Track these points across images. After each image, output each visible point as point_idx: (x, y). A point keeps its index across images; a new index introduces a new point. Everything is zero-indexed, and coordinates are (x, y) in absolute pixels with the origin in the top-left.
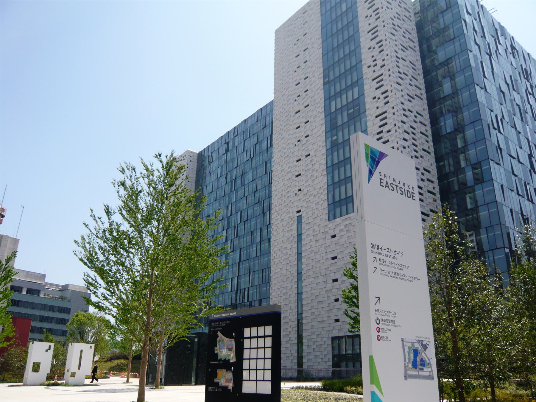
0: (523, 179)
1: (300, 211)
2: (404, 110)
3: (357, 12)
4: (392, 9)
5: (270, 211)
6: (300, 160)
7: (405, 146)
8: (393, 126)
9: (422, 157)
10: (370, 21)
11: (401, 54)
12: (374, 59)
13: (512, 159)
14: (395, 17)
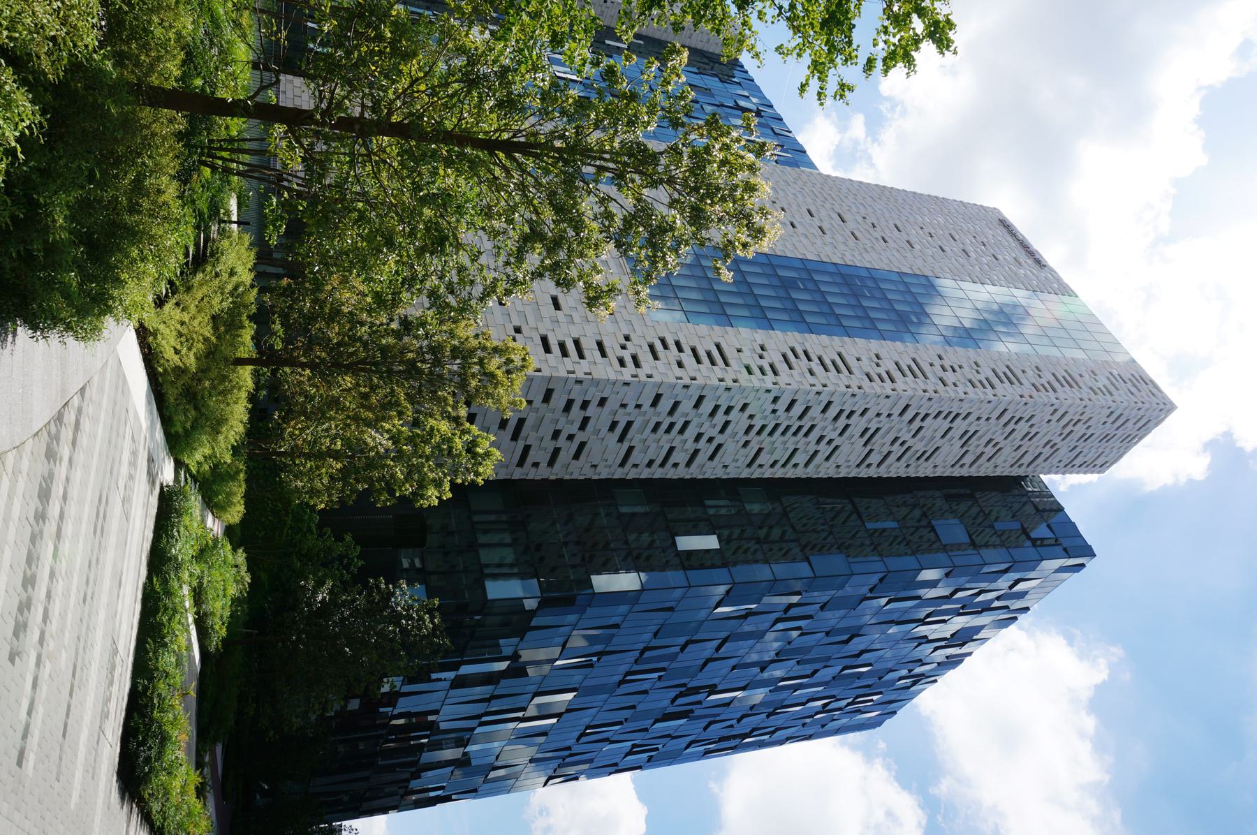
0: (674, 665)
2: (585, 405)
7: (780, 402)
8: (693, 375)
9: (746, 444)
12: (957, 368)
13: (716, 643)
14: (1032, 426)
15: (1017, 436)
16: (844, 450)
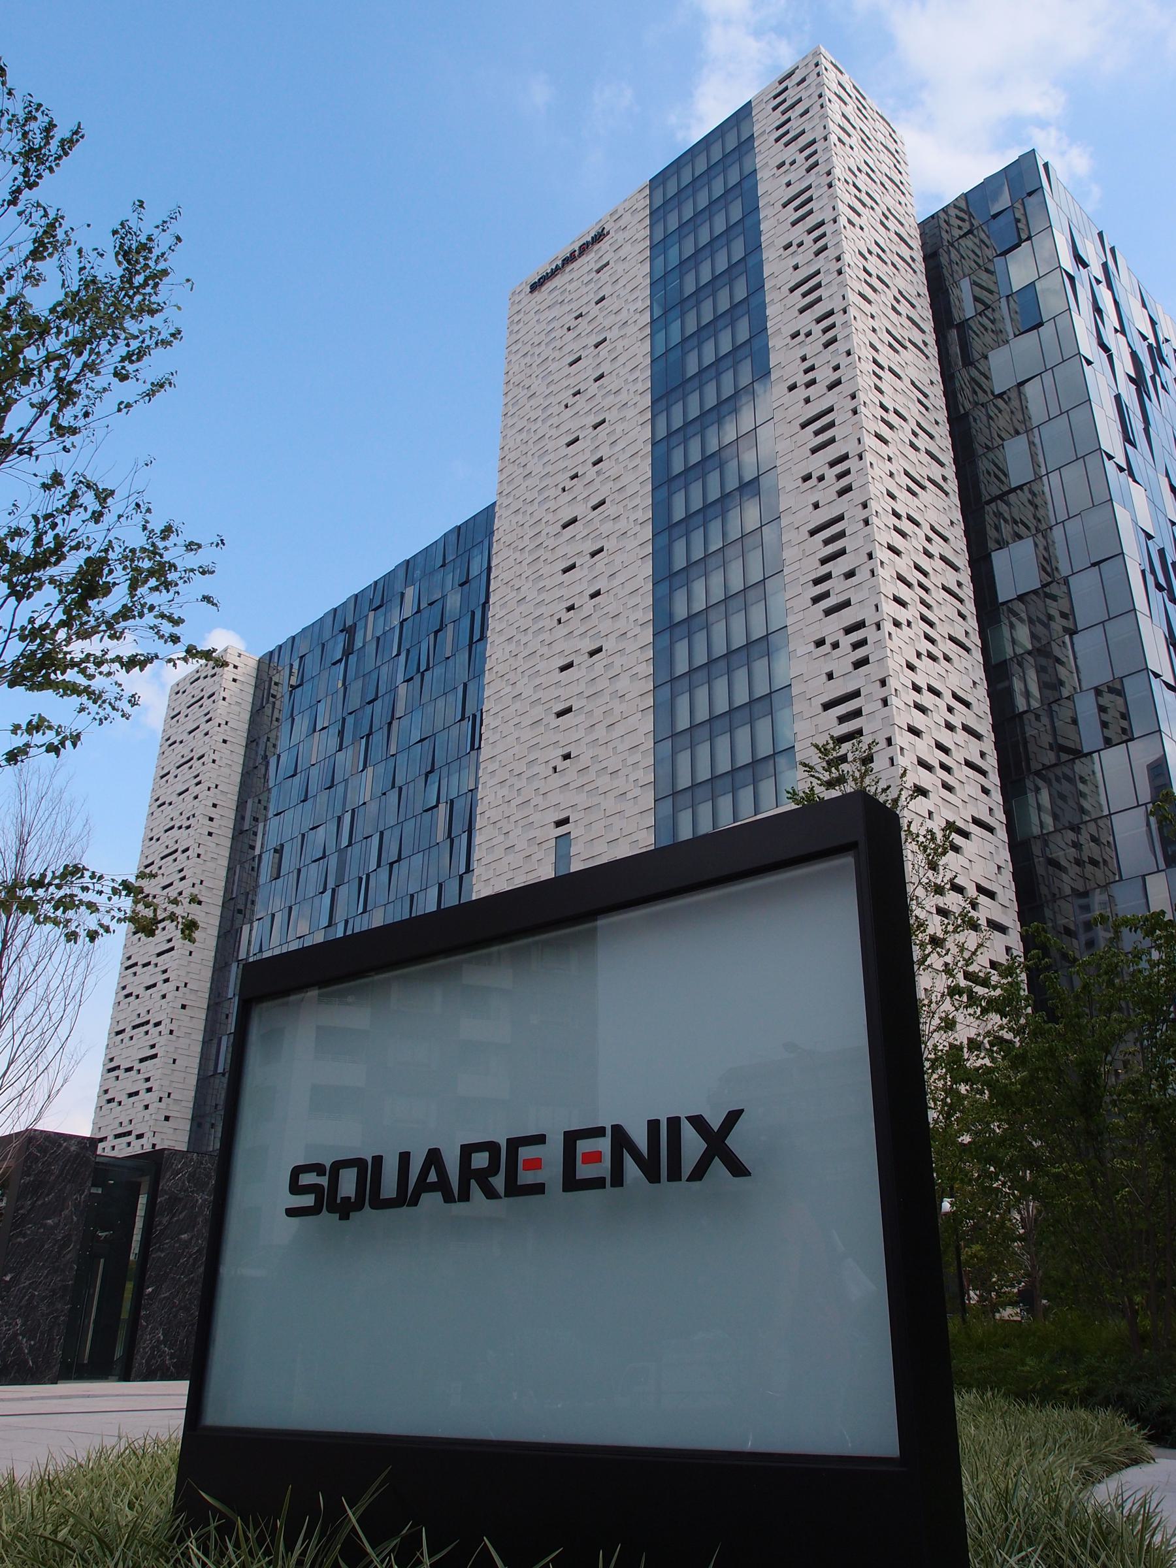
1: (566, 821)
2: (917, 689)
3: (760, 233)
4: (862, 228)
5: (470, 831)
6: (570, 665)
9: (947, 659)
10: (799, 259)
11: (886, 356)
12: (807, 364)
14: (870, 252)
15: (884, 271)
16: (902, 285)
